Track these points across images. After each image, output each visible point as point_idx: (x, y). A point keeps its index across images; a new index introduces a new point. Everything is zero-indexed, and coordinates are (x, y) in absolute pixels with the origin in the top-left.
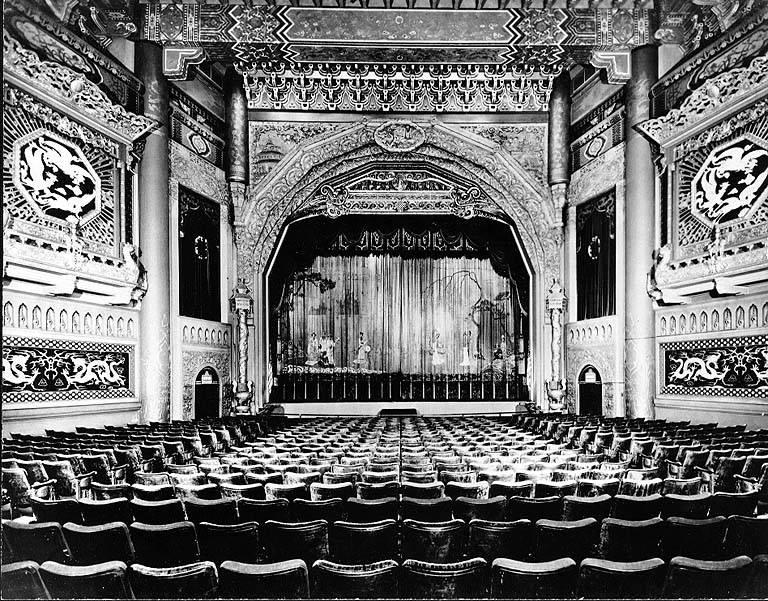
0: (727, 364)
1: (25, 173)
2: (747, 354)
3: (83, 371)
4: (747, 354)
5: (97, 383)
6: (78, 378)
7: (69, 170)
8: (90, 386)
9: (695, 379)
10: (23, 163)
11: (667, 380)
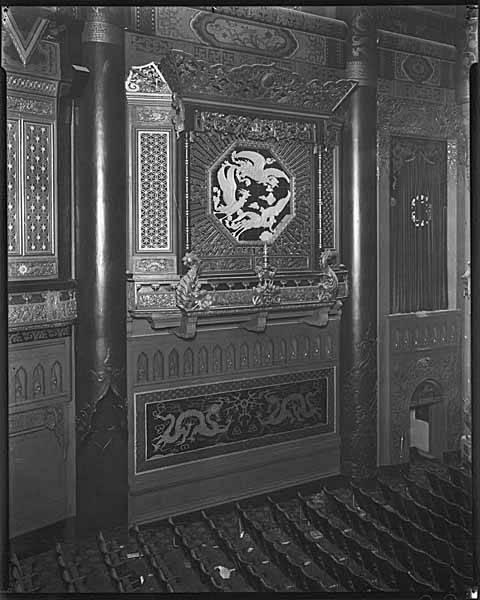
0: (230, 414)
1: (217, 200)
2: (251, 400)
3: (276, 411)
4: (251, 400)
5: (292, 421)
6: (272, 420)
7: (262, 179)
8: (286, 426)
9: (192, 439)
10: (215, 189)
11: (151, 448)
